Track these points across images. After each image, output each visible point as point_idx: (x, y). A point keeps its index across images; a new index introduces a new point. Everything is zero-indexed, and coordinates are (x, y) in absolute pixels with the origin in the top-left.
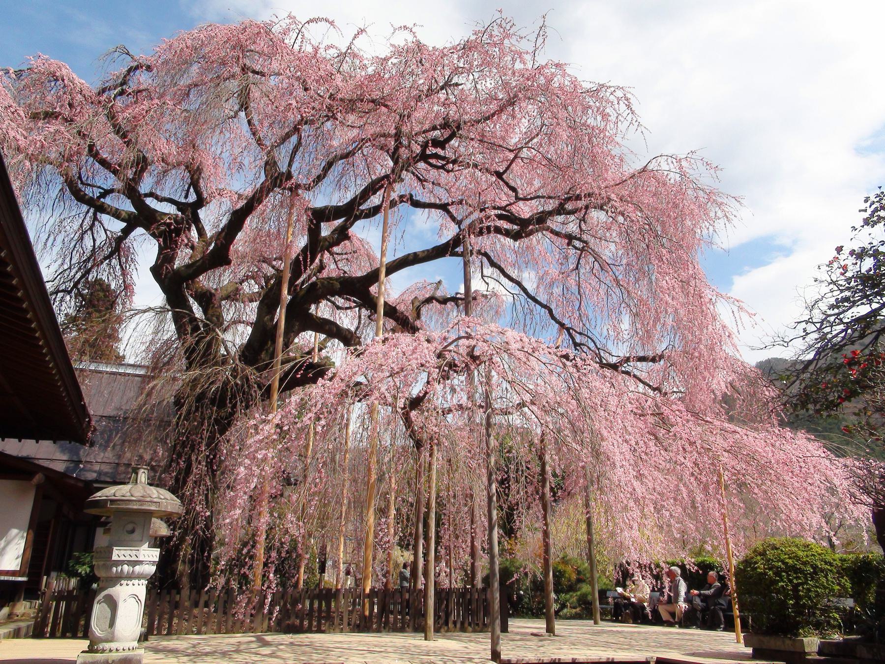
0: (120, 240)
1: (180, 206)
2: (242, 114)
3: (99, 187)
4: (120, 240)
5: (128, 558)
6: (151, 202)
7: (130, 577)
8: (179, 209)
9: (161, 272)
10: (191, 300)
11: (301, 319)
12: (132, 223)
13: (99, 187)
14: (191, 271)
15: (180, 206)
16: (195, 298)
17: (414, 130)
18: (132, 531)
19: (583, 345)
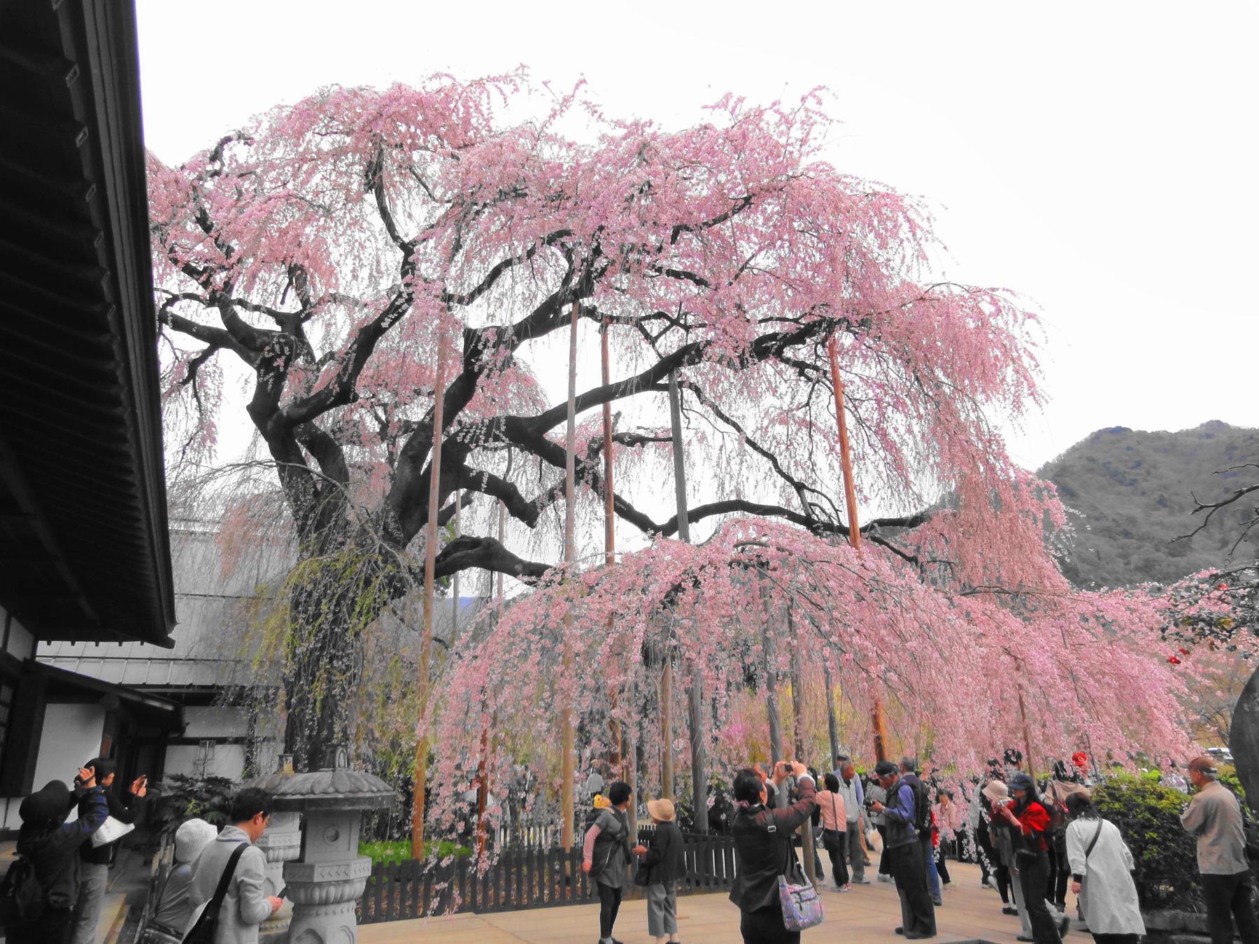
0: (194, 365)
1: (280, 318)
2: (371, 197)
3: (166, 292)
4: (194, 365)
5: (335, 878)
6: (243, 315)
7: (338, 901)
8: (278, 322)
9: (263, 410)
10: (304, 451)
11: (458, 475)
12: (215, 340)
13: (166, 292)
14: (304, 411)
15: (280, 318)
16: (302, 443)
17: (607, 231)
18: (336, 837)
19: (815, 505)
